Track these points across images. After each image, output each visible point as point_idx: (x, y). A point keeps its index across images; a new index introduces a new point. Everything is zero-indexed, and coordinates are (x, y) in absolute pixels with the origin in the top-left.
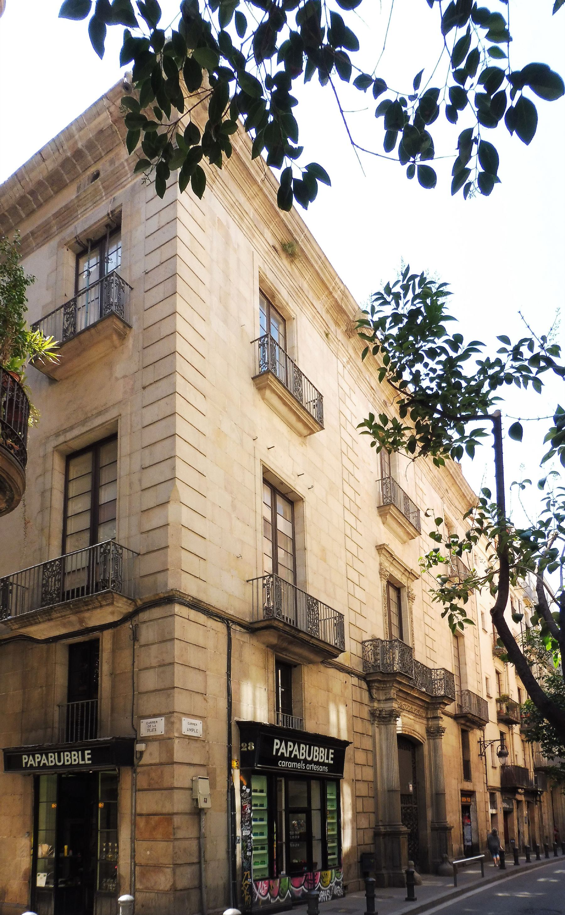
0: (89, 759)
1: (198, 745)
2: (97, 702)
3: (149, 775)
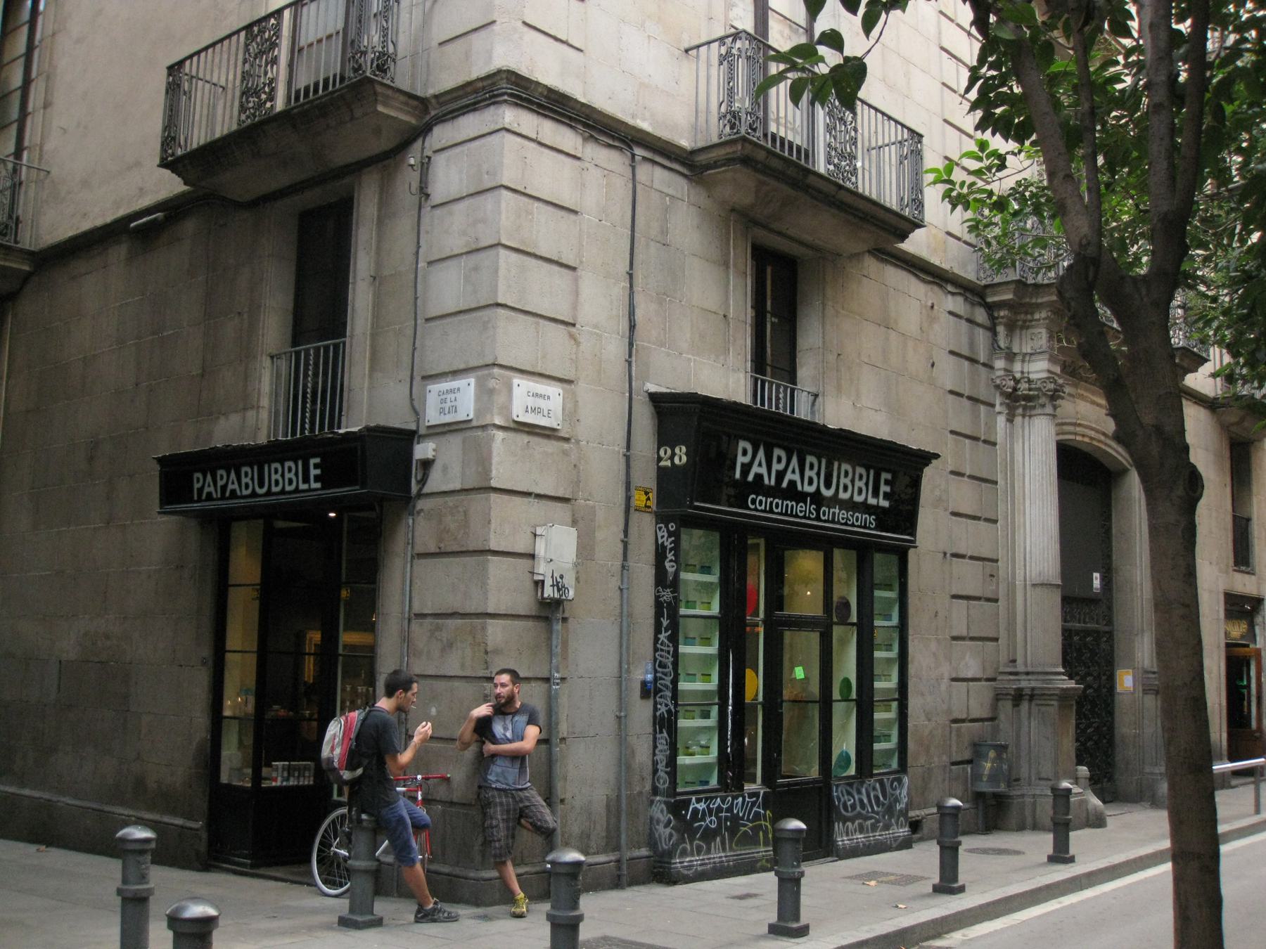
0: (317, 479)
1: (551, 446)
2: (344, 343)
3: (440, 522)
